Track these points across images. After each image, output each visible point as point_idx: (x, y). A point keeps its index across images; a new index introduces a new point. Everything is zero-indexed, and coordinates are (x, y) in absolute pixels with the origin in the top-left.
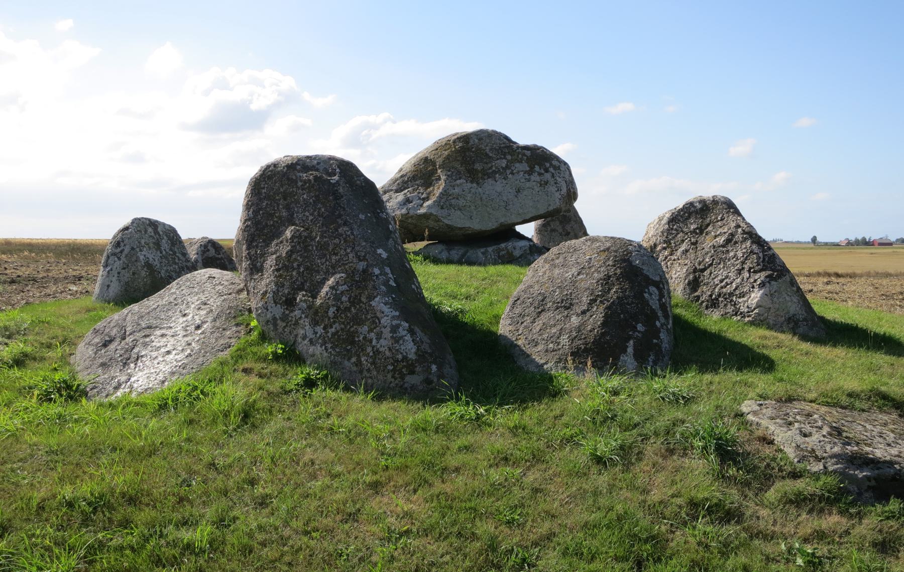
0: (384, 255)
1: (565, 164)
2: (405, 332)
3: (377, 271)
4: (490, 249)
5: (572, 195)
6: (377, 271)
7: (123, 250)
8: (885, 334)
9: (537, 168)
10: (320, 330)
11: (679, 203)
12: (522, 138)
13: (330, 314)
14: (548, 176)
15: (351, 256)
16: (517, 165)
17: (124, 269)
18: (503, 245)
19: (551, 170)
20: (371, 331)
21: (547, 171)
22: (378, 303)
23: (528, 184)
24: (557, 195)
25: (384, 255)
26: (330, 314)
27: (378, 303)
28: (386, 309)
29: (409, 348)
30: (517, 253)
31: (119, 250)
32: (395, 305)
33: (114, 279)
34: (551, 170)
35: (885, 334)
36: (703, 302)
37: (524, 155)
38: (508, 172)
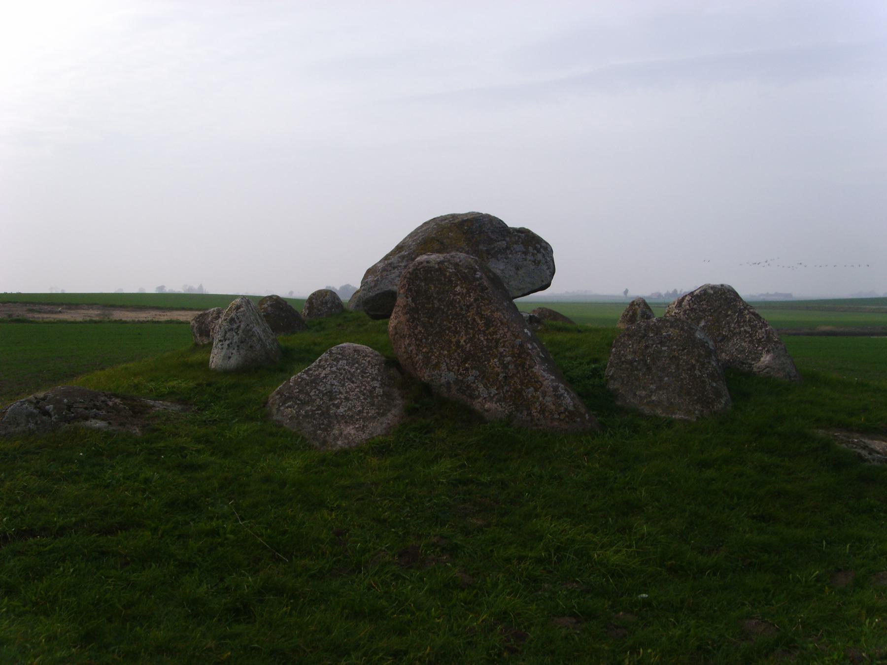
2: (563, 391)
3: (530, 346)
6: (530, 346)
7: (239, 326)
8: (675, 291)
10: (494, 391)
11: (462, 207)
12: (512, 222)
13: (500, 378)
14: (539, 257)
15: (508, 335)
16: (515, 246)
17: (242, 342)
20: (536, 390)
21: (539, 251)
22: (539, 369)
23: (525, 263)
26: (500, 378)
27: (539, 369)
28: (545, 374)
31: (235, 326)
32: (551, 371)
33: (234, 352)
34: (542, 250)
35: (675, 291)
36: (555, 389)
37: (519, 237)
38: (508, 252)
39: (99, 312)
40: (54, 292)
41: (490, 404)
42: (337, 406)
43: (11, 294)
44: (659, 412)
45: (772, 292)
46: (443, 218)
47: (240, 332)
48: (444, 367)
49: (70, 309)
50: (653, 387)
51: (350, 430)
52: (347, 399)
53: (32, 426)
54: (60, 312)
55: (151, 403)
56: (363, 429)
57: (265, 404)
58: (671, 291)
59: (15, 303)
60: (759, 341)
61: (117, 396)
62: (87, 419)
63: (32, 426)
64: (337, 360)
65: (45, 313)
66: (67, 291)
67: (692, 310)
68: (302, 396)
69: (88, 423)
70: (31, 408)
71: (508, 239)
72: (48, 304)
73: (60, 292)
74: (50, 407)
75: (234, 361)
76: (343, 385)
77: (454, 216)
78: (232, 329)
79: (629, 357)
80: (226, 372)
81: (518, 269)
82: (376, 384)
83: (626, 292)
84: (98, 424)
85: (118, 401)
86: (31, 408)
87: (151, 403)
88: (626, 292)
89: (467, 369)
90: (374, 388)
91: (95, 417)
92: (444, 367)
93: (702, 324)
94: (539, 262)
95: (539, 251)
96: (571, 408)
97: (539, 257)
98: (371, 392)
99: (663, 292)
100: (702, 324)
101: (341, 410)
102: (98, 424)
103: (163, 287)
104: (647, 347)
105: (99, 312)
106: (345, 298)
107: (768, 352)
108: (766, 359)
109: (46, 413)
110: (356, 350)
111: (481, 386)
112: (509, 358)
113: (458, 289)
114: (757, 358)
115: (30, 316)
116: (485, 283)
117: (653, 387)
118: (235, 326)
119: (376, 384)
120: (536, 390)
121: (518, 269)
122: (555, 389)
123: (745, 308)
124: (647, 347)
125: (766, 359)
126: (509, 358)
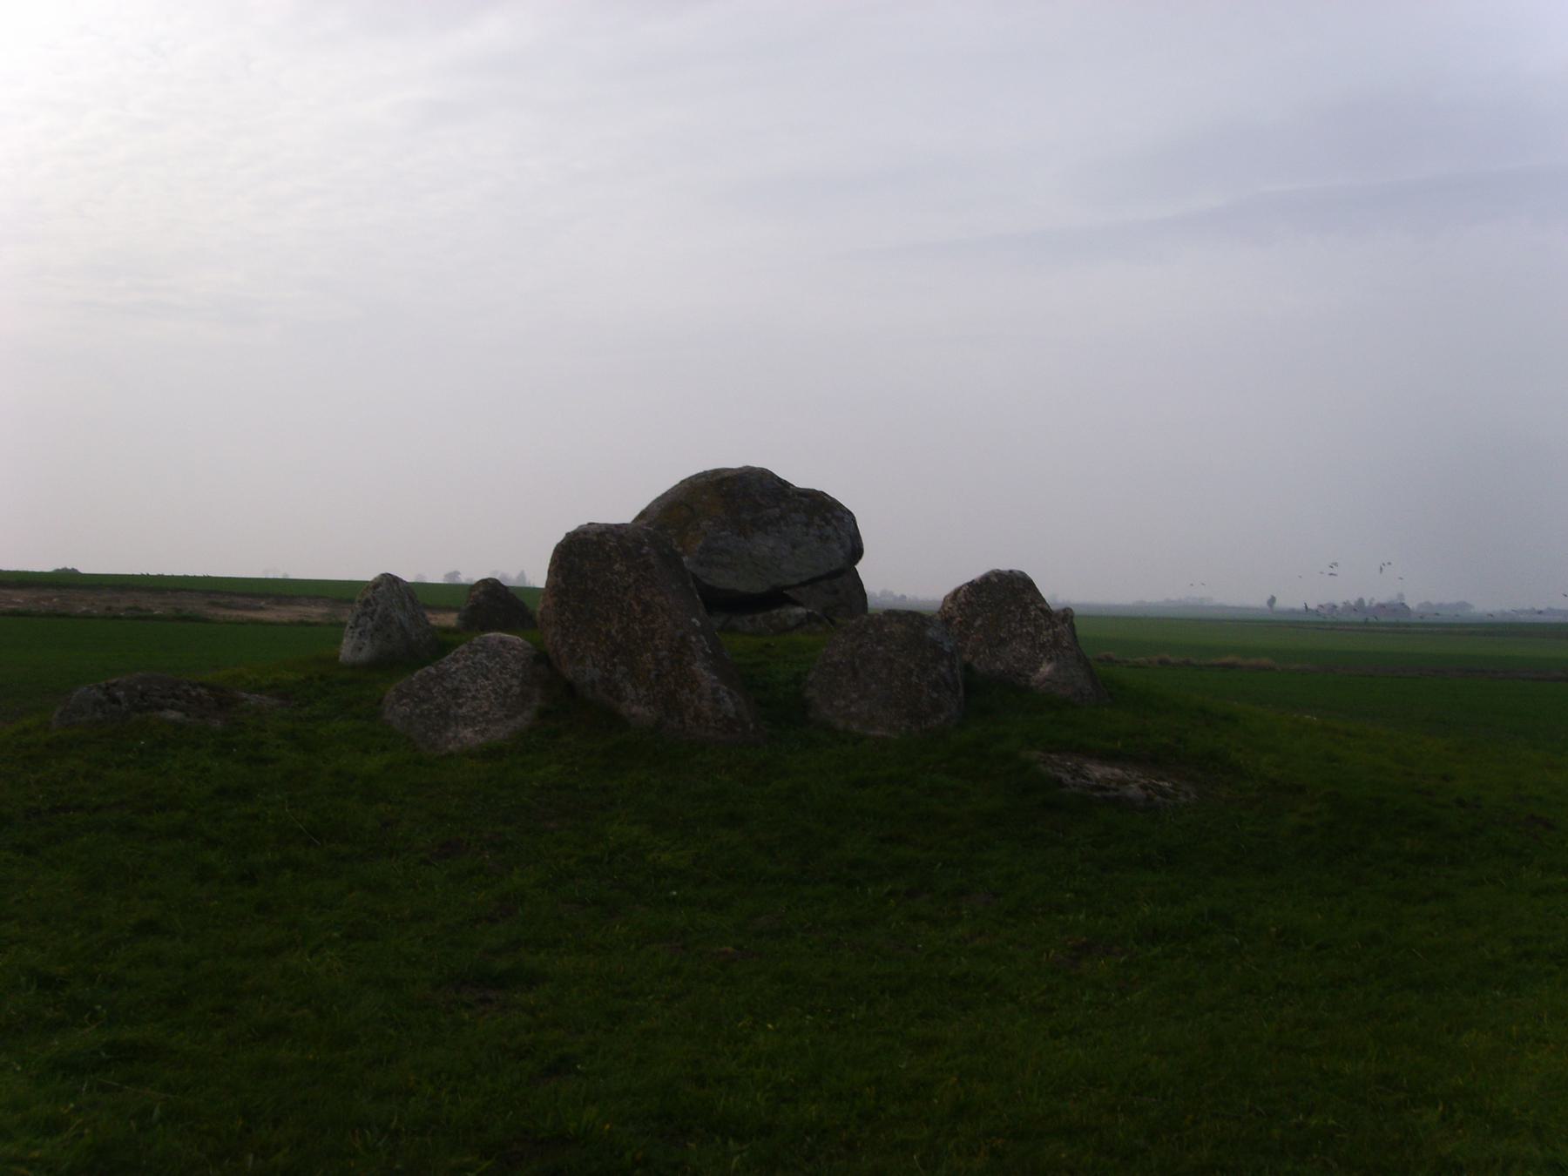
0: (698, 624)
1: (850, 513)
4: (759, 616)
5: (857, 552)
8: (1361, 601)
9: (817, 520)
10: (642, 691)
14: (829, 530)
18: (775, 612)
19: (834, 522)
21: (828, 523)
22: (699, 667)
24: (841, 553)
25: (698, 624)
27: (699, 667)
29: (729, 706)
30: (791, 623)
31: (370, 609)
34: (834, 522)
35: (1361, 601)
36: (715, 691)
39: (326, 610)
40: (271, 576)
41: (638, 709)
42: (460, 706)
43: (195, 578)
44: (855, 727)
45: (1507, 609)
46: (698, 476)
47: (376, 617)
48: (589, 662)
49: (278, 603)
50: (855, 696)
51: (468, 733)
52: (474, 698)
53: (99, 715)
54: (261, 608)
55: (244, 695)
56: (482, 732)
57: (380, 702)
58: (1353, 601)
59: (192, 591)
60: (1043, 646)
61: (202, 685)
62: (161, 708)
63: (99, 715)
64: (476, 652)
65: (236, 608)
66: (293, 576)
67: (969, 603)
68: (422, 693)
69: (162, 714)
70: (100, 695)
71: (783, 505)
72: (253, 595)
73: (280, 576)
74: (120, 694)
75: (363, 656)
76: (475, 682)
77: (705, 474)
78: (364, 614)
79: (836, 659)
80: (354, 667)
81: (794, 547)
82: (515, 682)
83: (1272, 600)
84: (173, 715)
85: (203, 691)
86: (100, 695)
87: (244, 695)
88: (1272, 600)
89: (614, 665)
90: (511, 686)
91: (172, 707)
92: (589, 662)
93: (978, 623)
94: (828, 538)
95: (828, 523)
96: (731, 715)
97: (829, 530)
98: (506, 691)
99: (1339, 602)
100: (978, 623)
101: (464, 710)
102: (173, 715)
103: (456, 574)
104: (860, 646)
105: (326, 610)
106: (871, 603)
107: (1050, 660)
108: (1046, 669)
109: (116, 701)
110: (503, 642)
111: (629, 686)
112: (665, 653)
113: (617, 566)
114: (1035, 670)
115: (211, 612)
116: (652, 561)
117: (855, 696)
118: (370, 609)
119: (515, 682)
120: (692, 692)
121: (794, 547)
122: (715, 691)
123: (1033, 602)
124: (860, 646)
125: (1046, 669)
126: (665, 653)
